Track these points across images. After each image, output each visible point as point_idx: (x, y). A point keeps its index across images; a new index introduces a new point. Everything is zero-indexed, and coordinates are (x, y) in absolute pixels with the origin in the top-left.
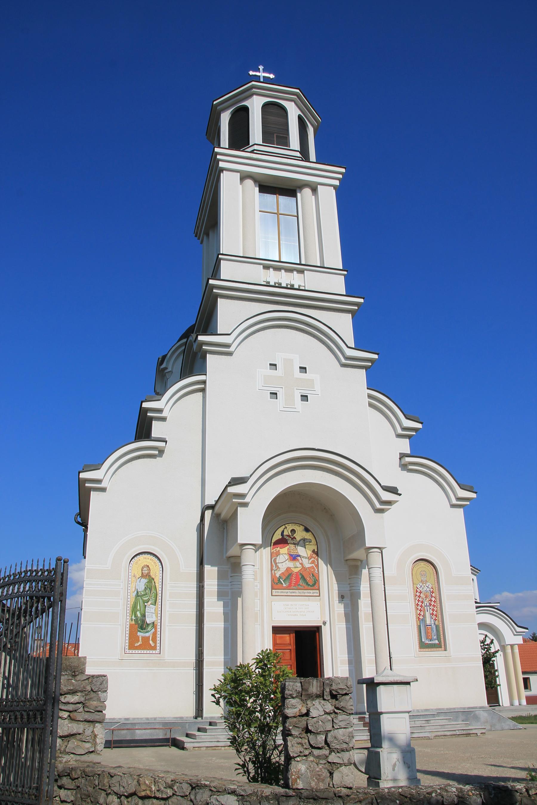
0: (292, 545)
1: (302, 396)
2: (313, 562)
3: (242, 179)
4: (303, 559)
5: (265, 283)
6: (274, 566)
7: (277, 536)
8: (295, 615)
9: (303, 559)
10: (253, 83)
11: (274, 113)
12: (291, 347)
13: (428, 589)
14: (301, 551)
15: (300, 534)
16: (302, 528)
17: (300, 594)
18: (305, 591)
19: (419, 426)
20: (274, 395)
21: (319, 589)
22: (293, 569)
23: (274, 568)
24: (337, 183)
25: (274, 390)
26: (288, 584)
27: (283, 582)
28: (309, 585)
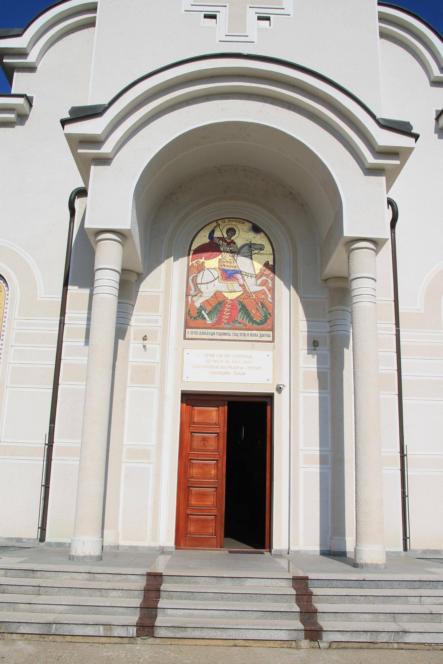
0: (228, 255)
2: (264, 283)
7: (203, 239)
8: (226, 373)
9: (245, 277)
14: (243, 263)
15: (243, 236)
17: (236, 338)
18: (246, 332)
22: (226, 295)
23: (192, 292)
26: (215, 319)
27: (206, 316)
28: (251, 320)
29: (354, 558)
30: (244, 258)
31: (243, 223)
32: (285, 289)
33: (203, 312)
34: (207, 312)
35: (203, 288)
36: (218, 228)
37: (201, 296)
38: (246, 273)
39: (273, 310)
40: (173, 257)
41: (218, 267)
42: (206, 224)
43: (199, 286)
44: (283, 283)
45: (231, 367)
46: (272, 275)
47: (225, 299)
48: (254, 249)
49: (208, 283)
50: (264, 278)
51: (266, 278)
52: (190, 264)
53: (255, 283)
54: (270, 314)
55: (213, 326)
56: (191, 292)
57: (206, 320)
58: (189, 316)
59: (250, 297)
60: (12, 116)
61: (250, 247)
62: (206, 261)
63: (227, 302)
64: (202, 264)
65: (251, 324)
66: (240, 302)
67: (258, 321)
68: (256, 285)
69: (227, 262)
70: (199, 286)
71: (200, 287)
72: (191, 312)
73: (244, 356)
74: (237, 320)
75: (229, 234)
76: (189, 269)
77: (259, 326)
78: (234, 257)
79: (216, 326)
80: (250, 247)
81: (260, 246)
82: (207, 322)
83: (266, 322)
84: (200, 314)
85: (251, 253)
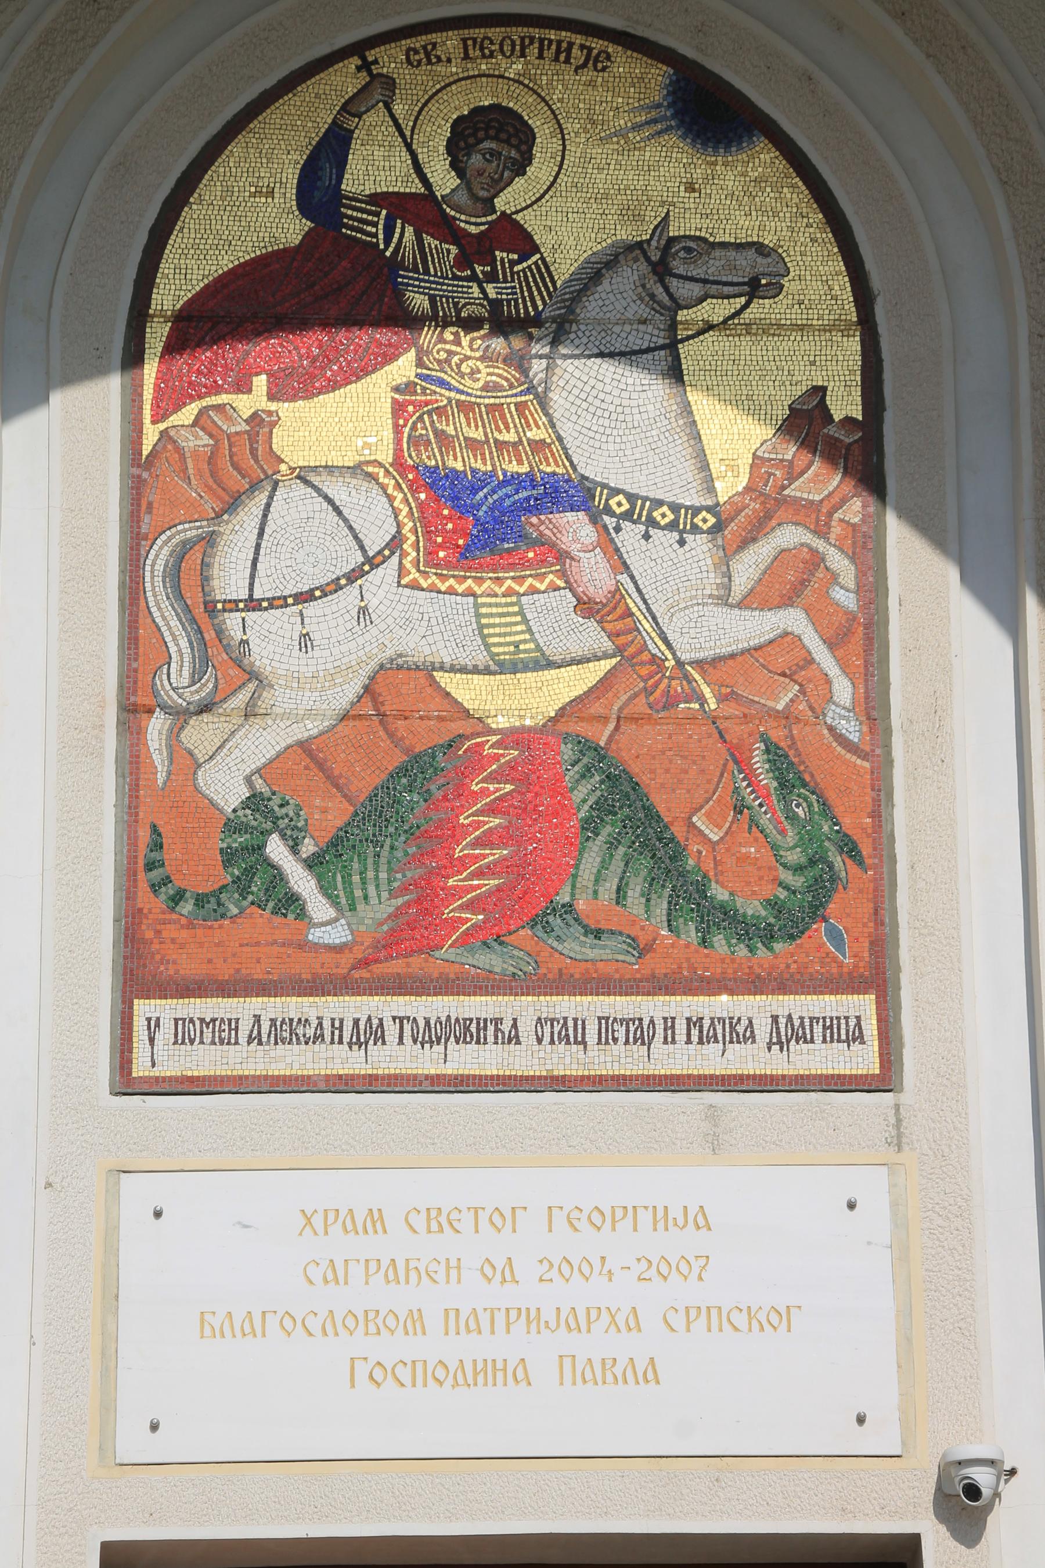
0: (470, 345)
2: (793, 583)
4: (629, 537)
6: (180, 644)
7: (248, 214)
8: (488, 1372)
9: (629, 537)
14: (601, 413)
15: (595, 183)
16: (634, 85)
17: (565, 1060)
18: (652, 1007)
21: (877, 978)
22: (469, 692)
23: (177, 680)
26: (379, 909)
27: (302, 881)
29: (416, 187)
30: (607, 368)
31: (595, 61)
32: (970, 625)
33: (276, 849)
34: (308, 848)
35: (267, 638)
36: (376, 117)
37: (249, 713)
38: (631, 498)
39: (880, 805)
40: (860, 418)
41: (386, 456)
42: (269, 82)
43: (232, 621)
44: (953, 574)
45: (532, 1318)
46: (856, 509)
47: (459, 727)
48: (697, 289)
49: (305, 597)
50: (790, 536)
51: (808, 538)
52: (151, 435)
53: (713, 579)
54: (850, 848)
55: (365, 963)
56: (162, 682)
57: (302, 914)
58: (155, 888)
59: (671, 702)
61: (661, 270)
62: (284, 409)
63: (477, 760)
64: (252, 437)
65: (691, 934)
66: (585, 746)
67: (752, 908)
68: (723, 599)
69: (465, 408)
70: (232, 621)
71: (237, 635)
72: (172, 854)
73: (645, 1218)
74: (569, 908)
75: (476, 160)
76: (140, 472)
77: (762, 952)
78: (520, 363)
79: (395, 966)
80: (661, 270)
81: (745, 261)
82: (315, 935)
83: (816, 910)
84: (247, 863)
85: (673, 326)
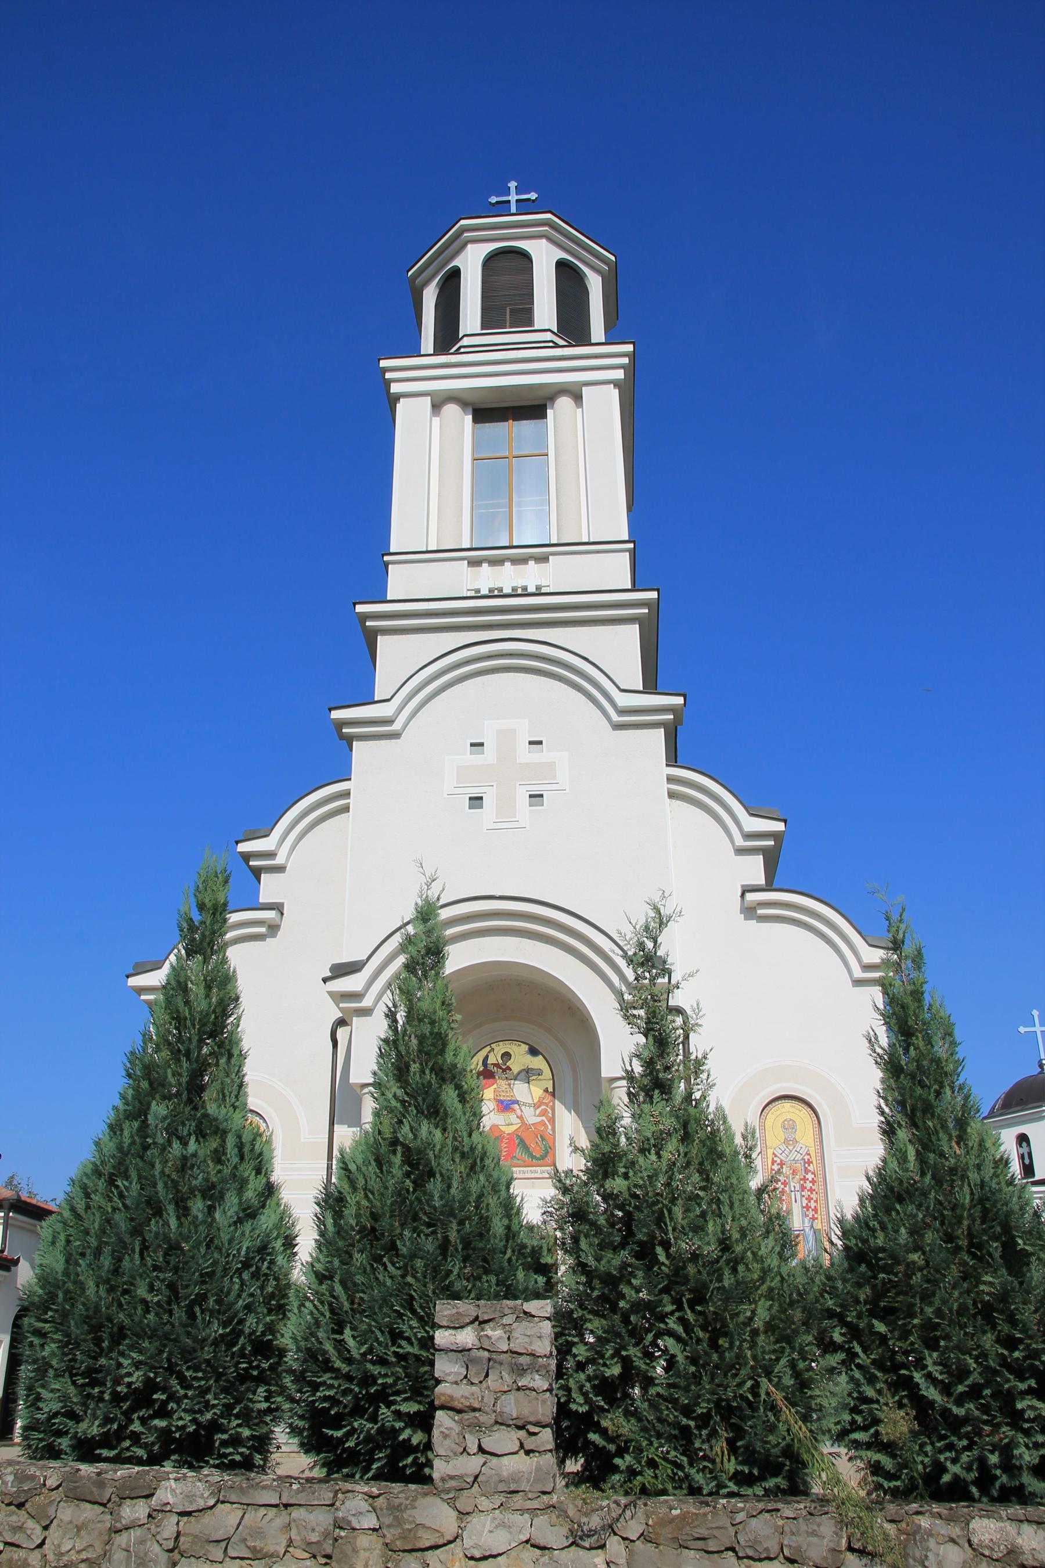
1: (531, 796)
2: (544, 1113)
3: (436, 407)
5: (473, 594)
9: (523, 1108)
10: (463, 222)
11: (508, 269)
12: (510, 705)
13: (799, 1157)
14: (521, 1091)
15: (521, 1058)
19: (780, 826)
20: (476, 801)
22: (503, 1128)
24: (620, 374)
25: (475, 792)
28: (533, 1157)
50: (543, 1107)
60: (263, 930)
